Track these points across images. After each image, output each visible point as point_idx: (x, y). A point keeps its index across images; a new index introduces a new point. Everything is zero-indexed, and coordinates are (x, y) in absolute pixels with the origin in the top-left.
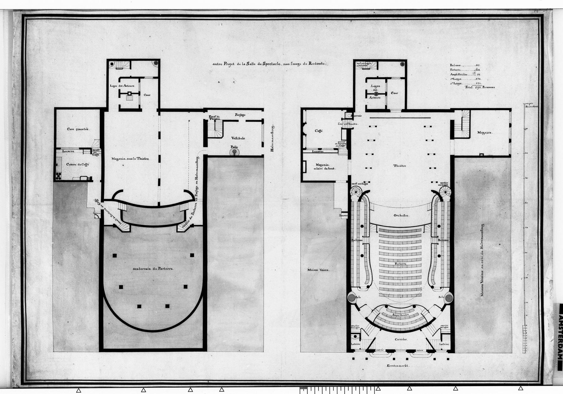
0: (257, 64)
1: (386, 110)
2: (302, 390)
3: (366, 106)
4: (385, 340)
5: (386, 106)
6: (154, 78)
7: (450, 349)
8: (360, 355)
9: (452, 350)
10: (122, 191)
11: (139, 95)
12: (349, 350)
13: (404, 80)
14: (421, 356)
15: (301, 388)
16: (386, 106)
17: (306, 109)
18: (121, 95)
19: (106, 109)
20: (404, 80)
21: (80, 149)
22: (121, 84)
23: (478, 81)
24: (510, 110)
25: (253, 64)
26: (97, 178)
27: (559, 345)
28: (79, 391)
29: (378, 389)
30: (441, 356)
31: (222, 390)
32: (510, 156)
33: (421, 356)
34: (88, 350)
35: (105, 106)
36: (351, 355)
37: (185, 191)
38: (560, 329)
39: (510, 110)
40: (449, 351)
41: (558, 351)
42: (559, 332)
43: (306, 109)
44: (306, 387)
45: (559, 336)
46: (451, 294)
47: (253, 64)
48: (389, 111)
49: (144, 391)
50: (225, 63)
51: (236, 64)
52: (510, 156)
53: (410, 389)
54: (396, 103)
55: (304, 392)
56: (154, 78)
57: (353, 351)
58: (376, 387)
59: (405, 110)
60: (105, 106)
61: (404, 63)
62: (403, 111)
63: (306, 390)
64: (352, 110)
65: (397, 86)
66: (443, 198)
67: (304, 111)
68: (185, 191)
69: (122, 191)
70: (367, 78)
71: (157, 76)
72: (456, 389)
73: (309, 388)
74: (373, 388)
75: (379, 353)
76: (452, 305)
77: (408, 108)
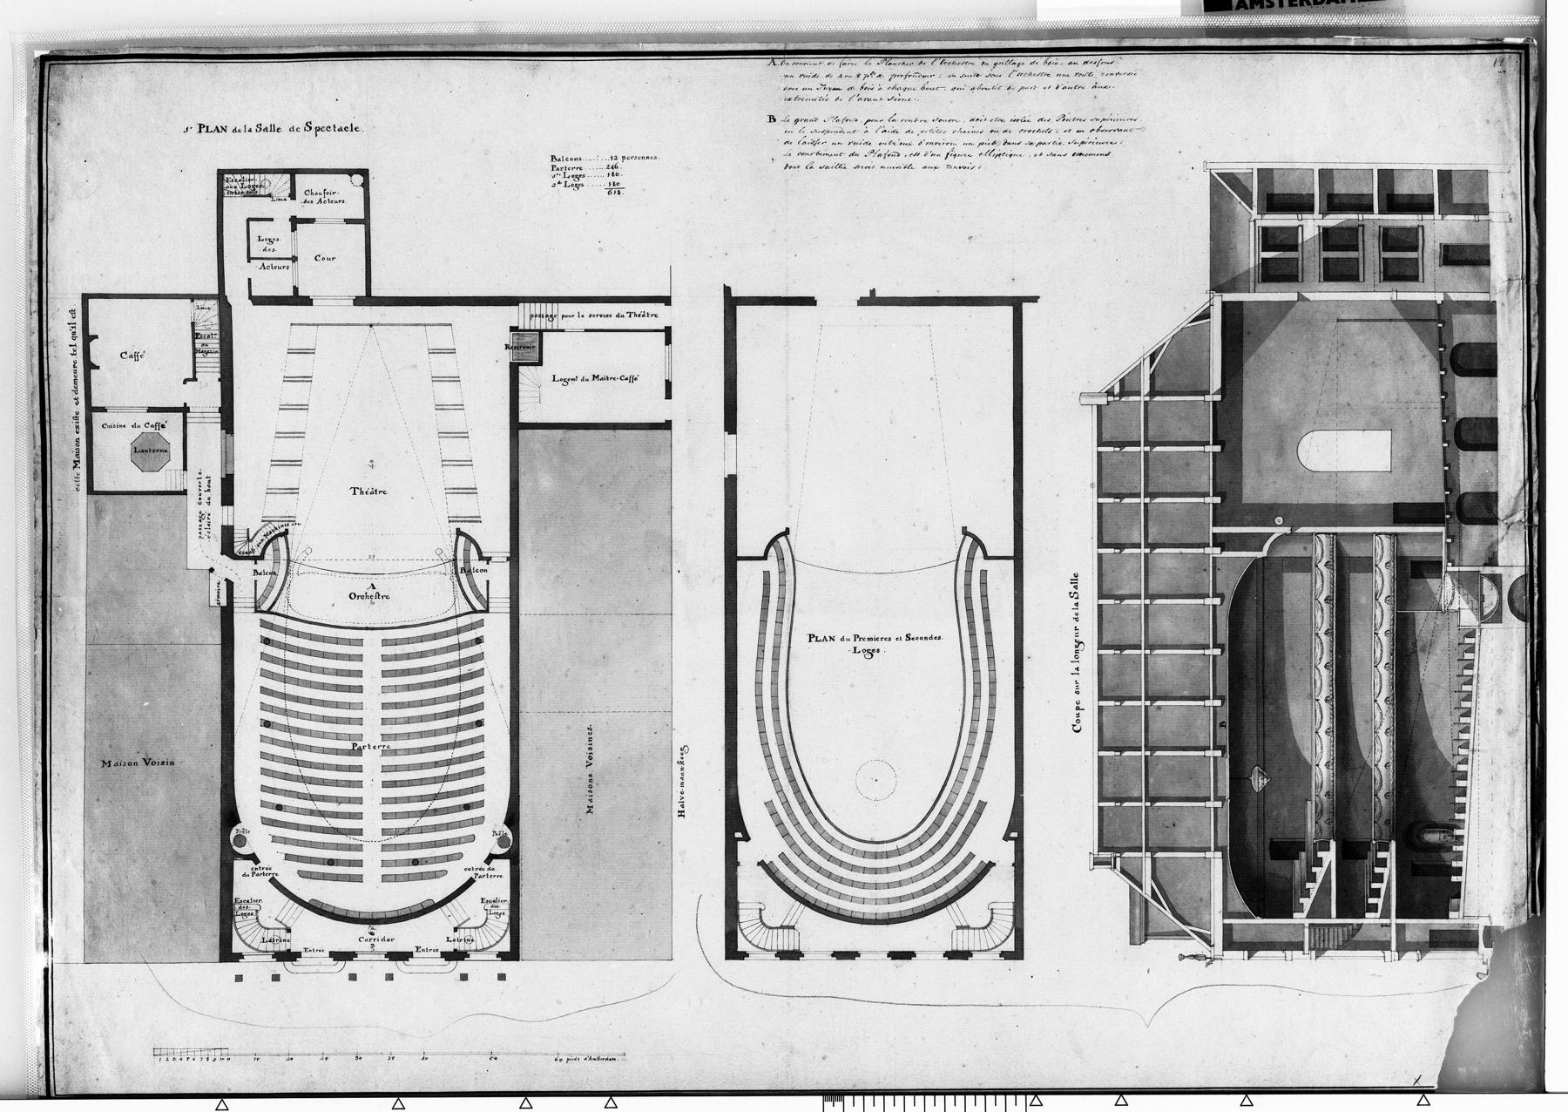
2: (828, 1104)
3: (1034, 299)
5: (296, 289)
8: (257, 969)
9: (513, 955)
12: (227, 954)
14: (426, 969)
16: (296, 289)
23: (616, 179)
25: (274, 129)
29: (1036, 1102)
30: (482, 969)
33: (426, 969)
34: (194, 958)
36: (232, 968)
40: (503, 956)
46: (510, 836)
47: (274, 129)
48: (307, 301)
50: (308, 125)
51: (229, 130)
57: (238, 957)
58: (1030, 1098)
62: (358, 301)
63: (839, 1104)
74: (1021, 1098)
75: (311, 961)
76: (514, 857)
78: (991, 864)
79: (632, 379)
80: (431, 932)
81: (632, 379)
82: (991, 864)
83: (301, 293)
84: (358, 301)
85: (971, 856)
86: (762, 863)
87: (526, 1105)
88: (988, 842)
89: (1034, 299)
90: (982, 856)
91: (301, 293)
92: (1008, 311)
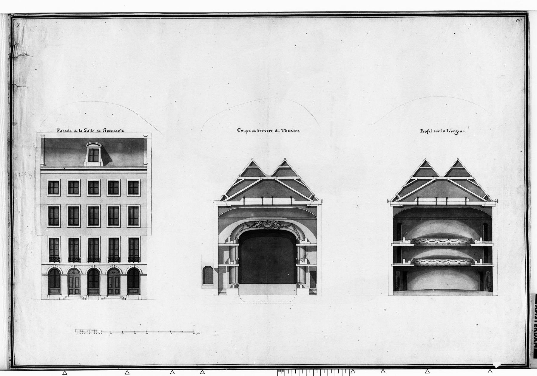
0: (73, 131)
2: (279, 373)
15: (279, 370)
26: (60, 263)
27: (535, 334)
28: (127, 373)
29: (353, 372)
31: (202, 373)
38: (536, 318)
41: (534, 340)
42: (535, 321)
43: (12, 359)
44: (284, 370)
45: (535, 325)
49: (65, 373)
53: (383, 372)
55: (281, 375)
58: (351, 370)
63: (283, 373)
66: (78, 335)
72: (490, 372)
73: (286, 371)
74: (348, 371)
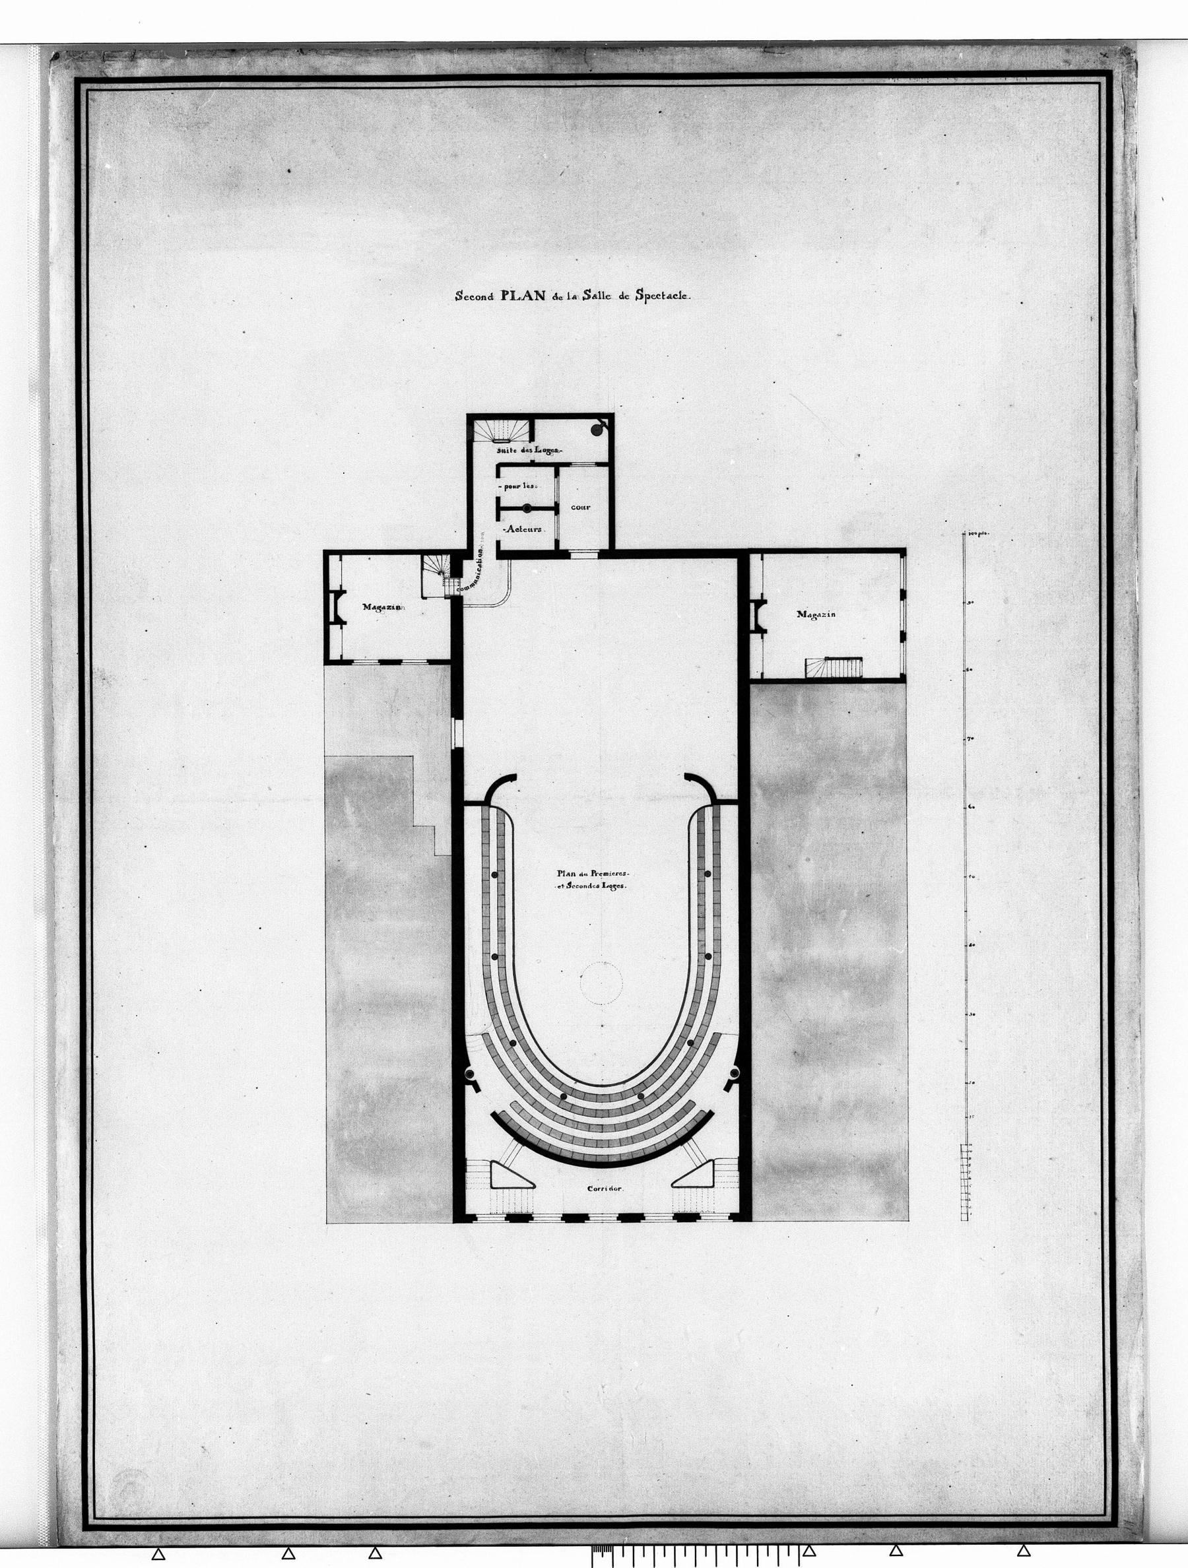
1: (559, 554)
2: (597, 1555)
3: (498, 543)
4: (561, 1187)
5: (557, 542)
6: (599, 464)
7: (737, 1210)
9: (744, 1214)
10: (512, 778)
11: (557, 512)
12: (461, 1215)
13: (606, 469)
16: (557, 542)
17: (341, 553)
18: (503, 513)
19: (468, 553)
20: (606, 469)
21: (349, 662)
22: (503, 482)
24: (902, 552)
29: (809, 1552)
32: (903, 679)
34: (435, 1217)
35: (464, 546)
37: (689, 777)
39: (902, 552)
52: (903, 679)
54: (583, 532)
56: (599, 464)
57: (472, 1218)
58: (803, 1548)
59: (611, 553)
60: (464, 546)
61: (605, 422)
62: (603, 554)
63: (608, 1555)
64: (458, 558)
65: (583, 486)
67: (333, 559)
68: (689, 777)
69: (512, 778)
70: (499, 466)
71: (605, 459)
74: (794, 1549)
77: (620, 545)
78: (710, 1114)
79: (802, 614)
80: (645, 1186)
81: (802, 614)
82: (710, 1114)
83: (562, 547)
84: (603, 554)
85: (691, 1104)
86: (494, 1115)
87: (289, 1555)
88: (712, 1090)
89: (498, 543)
90: (703, 1106)
91: (562, 547)
92: (732, 564)
